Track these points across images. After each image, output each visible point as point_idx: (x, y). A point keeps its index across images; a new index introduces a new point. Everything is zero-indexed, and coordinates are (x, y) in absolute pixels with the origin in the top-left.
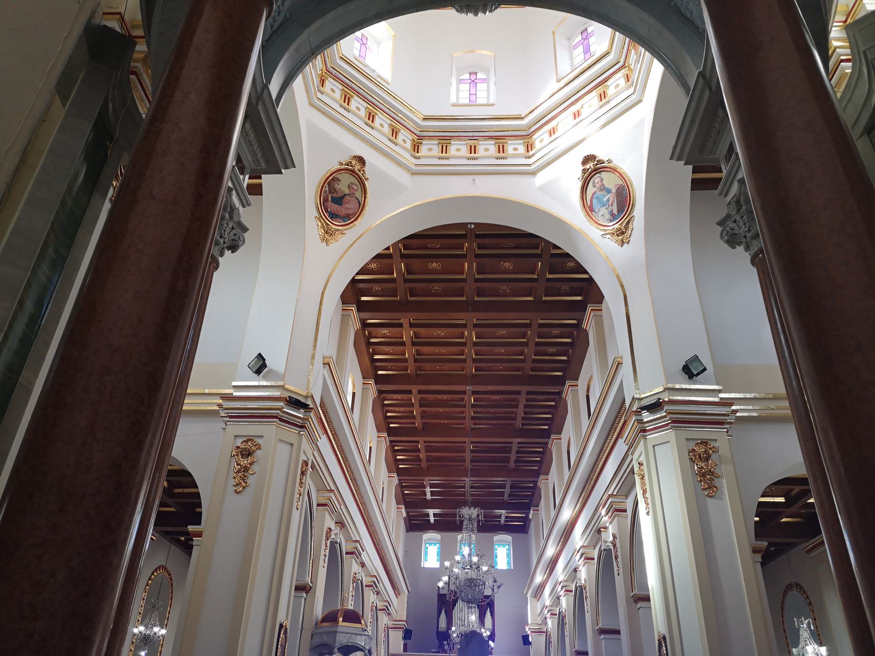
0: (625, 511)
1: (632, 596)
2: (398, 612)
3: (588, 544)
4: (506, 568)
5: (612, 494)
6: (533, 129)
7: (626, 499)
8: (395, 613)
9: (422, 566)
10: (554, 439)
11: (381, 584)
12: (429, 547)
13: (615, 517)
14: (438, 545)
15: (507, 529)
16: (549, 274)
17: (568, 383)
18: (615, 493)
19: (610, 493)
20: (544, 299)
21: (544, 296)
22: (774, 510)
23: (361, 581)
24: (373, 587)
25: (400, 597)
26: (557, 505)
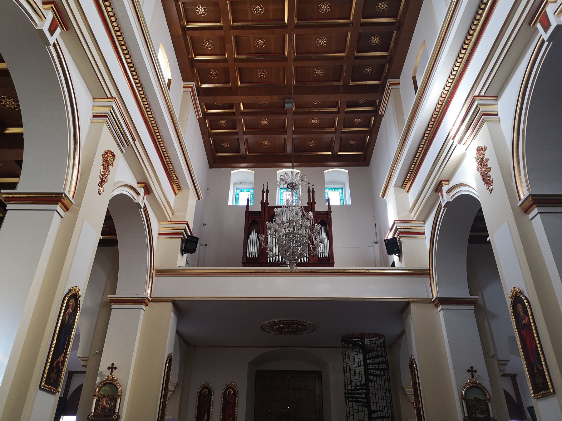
0: (423, 234)
1: (520, 206)
2: (176, 214)
3: (417, 218)
4: (339, 204)
5: (478, 96)
6: (311, 199)
7: (424, 223)
8: (170, 214)
9: (230, 203)
10: (390, 84)
11: (137, 142)
12: (241, 193)
13: (483, 121)
14: (252, 191)
15: (344, 162)
16: (351, 82)
17: (389, 81)
18: (482, 94)
19: (476, 94)
20: (351, 83)
21: (351, 82)
22: (356, 399)
23: (54, 45)
24: (108, 117)
25: (180, 194)
26: (419, 86)
